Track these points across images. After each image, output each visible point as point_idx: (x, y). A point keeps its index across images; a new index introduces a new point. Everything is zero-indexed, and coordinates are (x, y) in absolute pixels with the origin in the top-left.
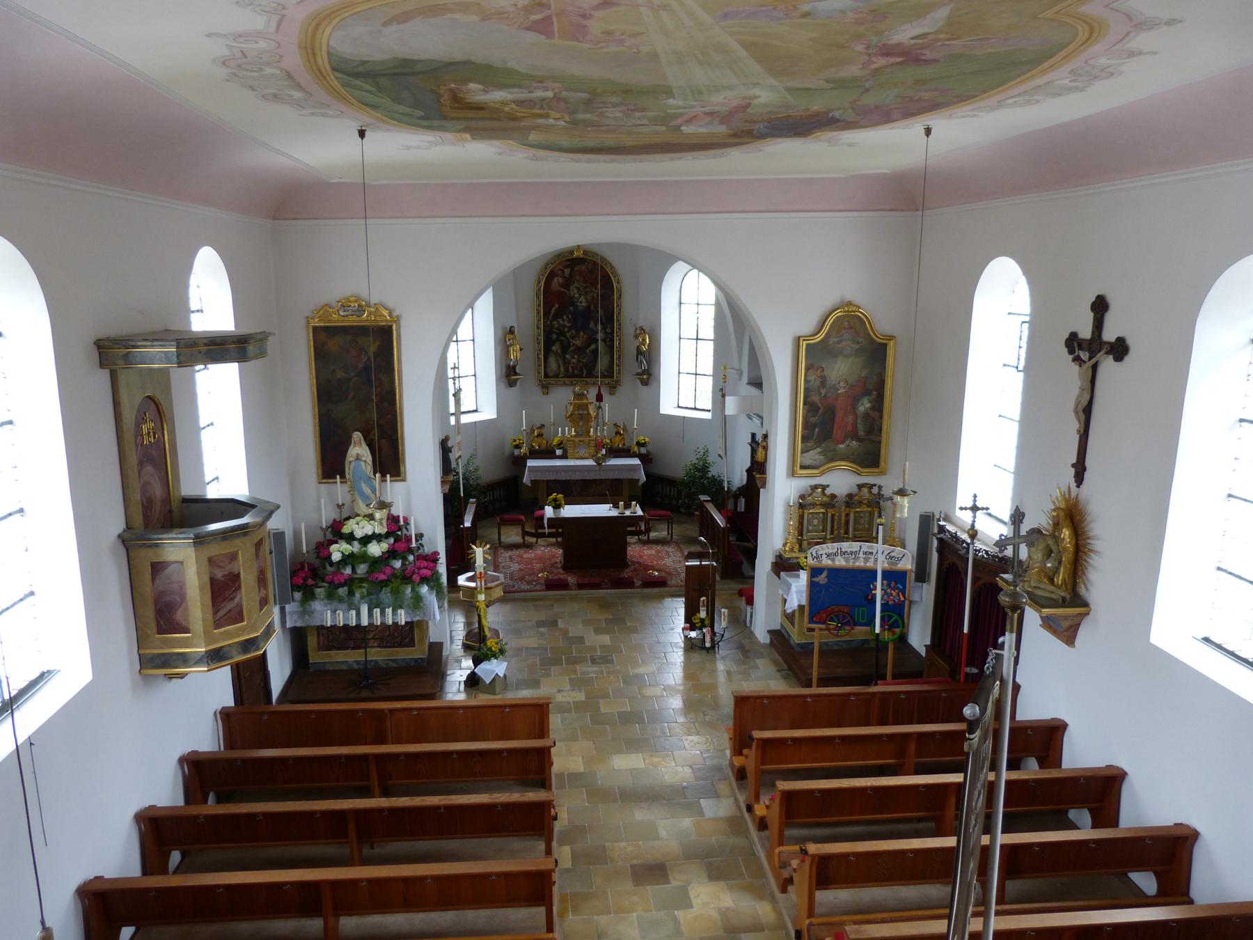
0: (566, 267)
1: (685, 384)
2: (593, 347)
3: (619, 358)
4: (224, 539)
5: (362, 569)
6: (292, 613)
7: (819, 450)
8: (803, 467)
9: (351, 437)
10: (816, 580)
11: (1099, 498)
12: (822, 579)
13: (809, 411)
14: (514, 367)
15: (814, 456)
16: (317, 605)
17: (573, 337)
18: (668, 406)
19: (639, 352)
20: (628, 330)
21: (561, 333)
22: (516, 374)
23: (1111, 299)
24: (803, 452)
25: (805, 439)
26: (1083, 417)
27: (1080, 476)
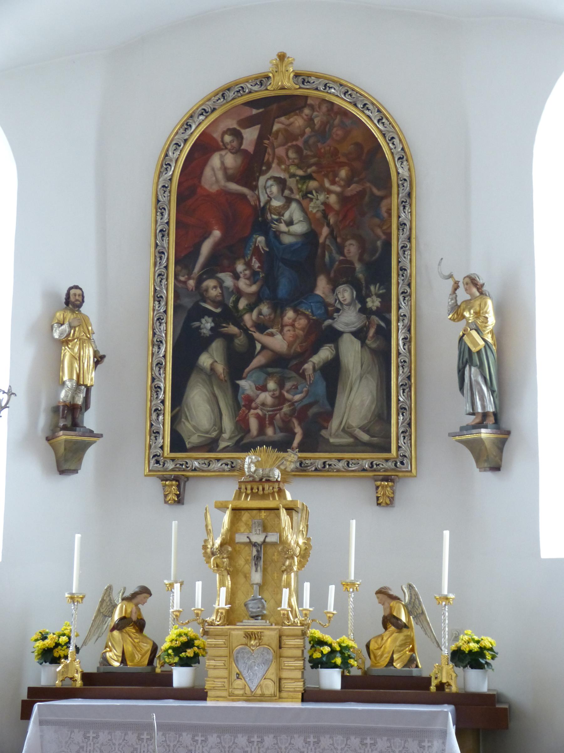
0: (248, 122)
2: (325, 353)
17: (262, 327)
21: (228, 314)
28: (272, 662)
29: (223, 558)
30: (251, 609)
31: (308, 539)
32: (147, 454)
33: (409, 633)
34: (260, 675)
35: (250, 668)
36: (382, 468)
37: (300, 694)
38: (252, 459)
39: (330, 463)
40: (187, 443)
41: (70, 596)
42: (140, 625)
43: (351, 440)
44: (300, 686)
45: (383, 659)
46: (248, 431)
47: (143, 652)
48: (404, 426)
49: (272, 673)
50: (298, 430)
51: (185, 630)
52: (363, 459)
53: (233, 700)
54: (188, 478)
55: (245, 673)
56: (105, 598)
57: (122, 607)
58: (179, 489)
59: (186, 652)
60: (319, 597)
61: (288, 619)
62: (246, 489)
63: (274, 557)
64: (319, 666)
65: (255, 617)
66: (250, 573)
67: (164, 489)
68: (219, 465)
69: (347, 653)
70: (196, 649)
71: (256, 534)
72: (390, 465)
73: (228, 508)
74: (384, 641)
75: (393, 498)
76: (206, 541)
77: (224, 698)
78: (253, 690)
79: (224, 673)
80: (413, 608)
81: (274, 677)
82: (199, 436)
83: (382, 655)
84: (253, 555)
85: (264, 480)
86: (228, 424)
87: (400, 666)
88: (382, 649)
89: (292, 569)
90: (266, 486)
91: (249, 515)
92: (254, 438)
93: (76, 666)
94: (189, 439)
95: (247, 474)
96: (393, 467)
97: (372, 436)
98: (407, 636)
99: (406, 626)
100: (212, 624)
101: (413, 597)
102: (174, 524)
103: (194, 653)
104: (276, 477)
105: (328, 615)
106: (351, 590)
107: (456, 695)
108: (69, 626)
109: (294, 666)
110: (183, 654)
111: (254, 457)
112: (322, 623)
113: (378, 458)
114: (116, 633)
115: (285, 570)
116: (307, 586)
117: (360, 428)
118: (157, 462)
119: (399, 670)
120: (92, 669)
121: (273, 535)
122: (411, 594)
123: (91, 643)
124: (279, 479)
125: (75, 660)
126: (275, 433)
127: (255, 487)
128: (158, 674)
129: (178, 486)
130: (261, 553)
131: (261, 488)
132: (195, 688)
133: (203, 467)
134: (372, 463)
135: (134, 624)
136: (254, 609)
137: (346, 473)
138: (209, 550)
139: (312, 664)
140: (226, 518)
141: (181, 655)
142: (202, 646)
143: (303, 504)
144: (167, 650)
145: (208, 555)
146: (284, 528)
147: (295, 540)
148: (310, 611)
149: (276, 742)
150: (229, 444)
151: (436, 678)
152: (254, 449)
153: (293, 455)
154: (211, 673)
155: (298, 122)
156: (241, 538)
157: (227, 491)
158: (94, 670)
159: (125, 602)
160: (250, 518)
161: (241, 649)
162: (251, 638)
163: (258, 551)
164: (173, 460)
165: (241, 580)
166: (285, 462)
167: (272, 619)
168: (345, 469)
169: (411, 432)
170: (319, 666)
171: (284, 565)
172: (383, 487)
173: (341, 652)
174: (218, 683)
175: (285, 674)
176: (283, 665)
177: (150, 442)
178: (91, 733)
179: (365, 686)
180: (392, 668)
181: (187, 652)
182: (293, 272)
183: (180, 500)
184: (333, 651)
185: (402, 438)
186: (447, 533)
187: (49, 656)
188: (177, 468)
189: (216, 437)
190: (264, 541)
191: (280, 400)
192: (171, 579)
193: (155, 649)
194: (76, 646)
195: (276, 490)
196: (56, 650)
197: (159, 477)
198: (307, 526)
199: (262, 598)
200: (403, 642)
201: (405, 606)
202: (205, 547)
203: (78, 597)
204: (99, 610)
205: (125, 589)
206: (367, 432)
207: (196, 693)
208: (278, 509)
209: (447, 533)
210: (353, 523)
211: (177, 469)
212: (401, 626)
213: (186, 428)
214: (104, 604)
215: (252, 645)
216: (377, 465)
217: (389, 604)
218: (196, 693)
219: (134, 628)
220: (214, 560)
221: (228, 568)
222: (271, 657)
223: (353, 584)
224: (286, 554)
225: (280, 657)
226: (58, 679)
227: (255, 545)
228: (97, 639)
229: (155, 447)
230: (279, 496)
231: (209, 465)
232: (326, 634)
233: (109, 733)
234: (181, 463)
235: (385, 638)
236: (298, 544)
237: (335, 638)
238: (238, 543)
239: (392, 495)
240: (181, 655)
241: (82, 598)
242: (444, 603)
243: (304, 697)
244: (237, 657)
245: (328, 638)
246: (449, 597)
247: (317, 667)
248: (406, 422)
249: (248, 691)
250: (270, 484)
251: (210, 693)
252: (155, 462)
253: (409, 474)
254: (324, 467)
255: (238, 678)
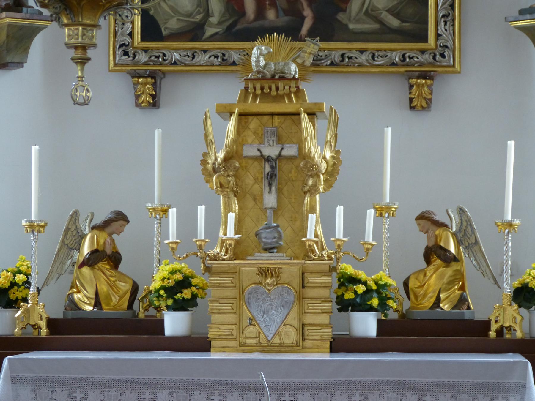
28: (293, 304)
29: (229, 176)
30: (264, 240)
31: (337, 152)
32: (112, 43)
33: (459, 268)
34: (278, 320)
35: (266, 312)
36: (417, 62)
37: (329, 342)
38: (261, 50)
39: (351, 55)
40: (163, 29)
41: (28, 224)
42: (115, 260)
43: (376, 26)
44: (328, 333)
45: (426, 299)
46: (242, 13)
47: (121, 292)
48: (445, 8)
49: (293, 318)
50: (308, 13)
51: (176, 266)
52: (392, 50)
53: (244, 351)
54: (164, 73)
55: (259, 318)
56: (70, 227)
57: (92, 238)
58: (155, 89)
59: (181, 292)
60: (354, 225)
61: (313, 251)
62: (255, 88)
63: (290, 175)
64: (350, 308)
65: (269, 250)
66: (262, 195)
67: (135, 88)
68: (207, 57)
69: (384, 293)
70: (194, 289)
71: (270, 145)
72: (428, 58)
73: (231, 114)
74: (427, 278)
75: (430, 100)
76: (205, 155)
77: (234, 349)
78: (269, 339)
79: (231, 318)
80: (466, 237)
81: (295, 323)
82: (178, 20)
83: (425, 295)
84: (268, 172)
85: (277, 77)
87: (447, 308)
88: (425, 287)
89: (317, 191)
90: (281, 85)
91: (258, 121)
92: (250, 23)
93: (39, 310)
94: (165, 23)
95: (255, 69)
96: (431, 60)
97: (403, 21)
98: (457, 270)
99: (455, 259)
100: (215, 258)
101: (465, 224)
102: (158, 133)
103: (192, 293)
104: (293, 73)
105: (366, 246)
106: (387, 215)
107: (522, 341)
108: (24, 261)
109: (321, 309)
110: (179, 295)
111: (263, 48)
112: (357, 257)
113: (412, 50)
114: (86, 270)
115: (309, 191)
116: (340, 210)
117: (388, 11)
118: (126, 53)
119: (447, 312)
120: (58, 314)
121: (291, 147)
122: (461, 219)
123: (52, 282)
124: (297, 76)
125: (37, 304)
126: (278, 17)
127: (266, 87)
128: (141, 320)
129: (154, 85)
130: (273, 170)
131: (274, 87)
132: (192, 336)
133: (187, 60)
134: (404, 56)
135: (106, 258)
136: (268, 239)
137: (373, 68)
138: (210, 166)
139: (339, 307)
140: (231, 125)
141: (175, 297)
142: (201, 285)
143: (331, 108)
144: (157, 291)
145: (209, 172)
146: (306, 138)
147: (320, 154)
148: (344, 241)
149: (34, 396)
150: (218, 30)
151: (496, 321)
152: (262, 37)
153: (312, 45)
154: (216, 318)
156: (250, 151)
157: (228, 90)
158: (60, 316)
159: (95, 231)
160: (260, 126)
161: (256, 288)
162: (266, 275)
163: (272, 167)
164: (146, 50)
165: (250, 203)
166: (302, 54)
167: (289, 252)
168: (369, 63)
169: (454, 16)
170: (350, 308)
171: (306, 184)
172: (418, 85)
173: (378, 291)
174: (225, 330)
175: (308, 319)
176: (306, 308)
177: (115, 27)
178: (78, 392)
179: (405, 332)
180: (438, 310)
181: (180, 293)
183: (155, 103)
184: (369, 291)
185: (443, 24)
186: (511, 144)
188: (151, 61)
189: (201, 20)
190: (280, 155)
192: (154, 202)
193: (135, 288)
195: (293, 89)
196: (12, 290)
197: (129, 73)
198: (336, 135)
199: (278, 226)
200: (452, 278)
201: (454, 234)
202: (204, 162)
203: (38, 225)
204: (63, 241)
205: (93, 214)
206: (397, 15)
207: (197, 343)
208: (298, 114)
209: (511, 144)
210: (389, 131)
211: (151, 63)
212: (448, 259)
214: (70, 234)
215: (268, 284)
216: (411, 58)
217: (434, 233)
218: (197, 343)
219: (109, 264)
220: (216, 178)
221: (235, 189)
222: (292, 298)
223: (388, 208)
224: (309, 170)
225: (303, 298)
226: (17, 326)
227: (268, 159)
228: (58, 278)
229: (123, 34)
230: (297, 97)
231: (193, 58)
232: (359, 269)
233: (101, 393)
234: (157, 54)
235: (429, 274)
236: (324, 158)
237: (369, 275)
238: (245, 157)
239: (430, 97)
240: (175, 297)
241: (43, 227)
242: (507, 231)
243: (333, 346)
244: (249, 298)
245: (362, 275)
246: (514, 223)
247: (346, 310)
248: (448, 3)
249: (263, 341)
250: (286, 82)
251: (213, 343)
252: (123, 53)
253: (451, 69)
254: (343, 60)
255: (251, 324)
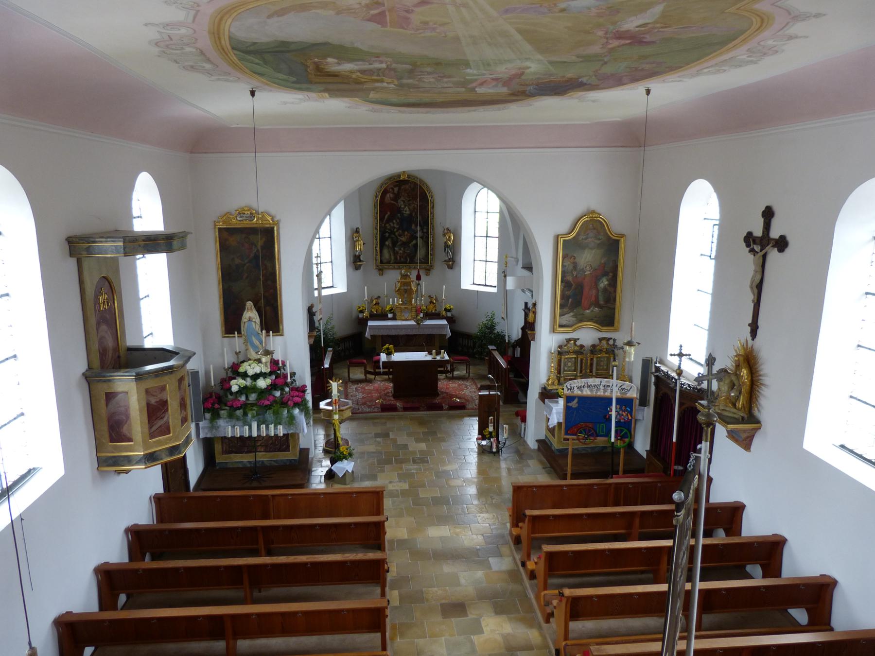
0: (395, 186)
1: (479, 268)
2: (414, 242)
3: (432, 250)
4: (157, 376)
5: (253, 397)
6: (204, 428)
7: (572, 314)
8: (561, 326)
9: (245, 305)
10: (570, 404)
11: (767, 348)
12: (574, 404)
13: (565, 287)
14: (359, 256)
15: (568, 318)
16: (221, 422)
17: (400, 235)
18: (466, 284)
19: (446, 246)
20: (439, 230)
21: (392, 233)
22: (360, 261)
23: (776, 209)
24: (560, 316)
25: (562, 306)
26: (756, 291)
27: (754, 332)
86: (392, 257)
155: (407, 187)
182: (407, 223)
187: (361, 312)
191: (404, 252)
194: (189, 233)
213: (383, 258)
